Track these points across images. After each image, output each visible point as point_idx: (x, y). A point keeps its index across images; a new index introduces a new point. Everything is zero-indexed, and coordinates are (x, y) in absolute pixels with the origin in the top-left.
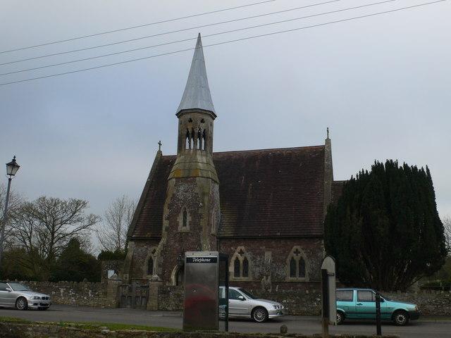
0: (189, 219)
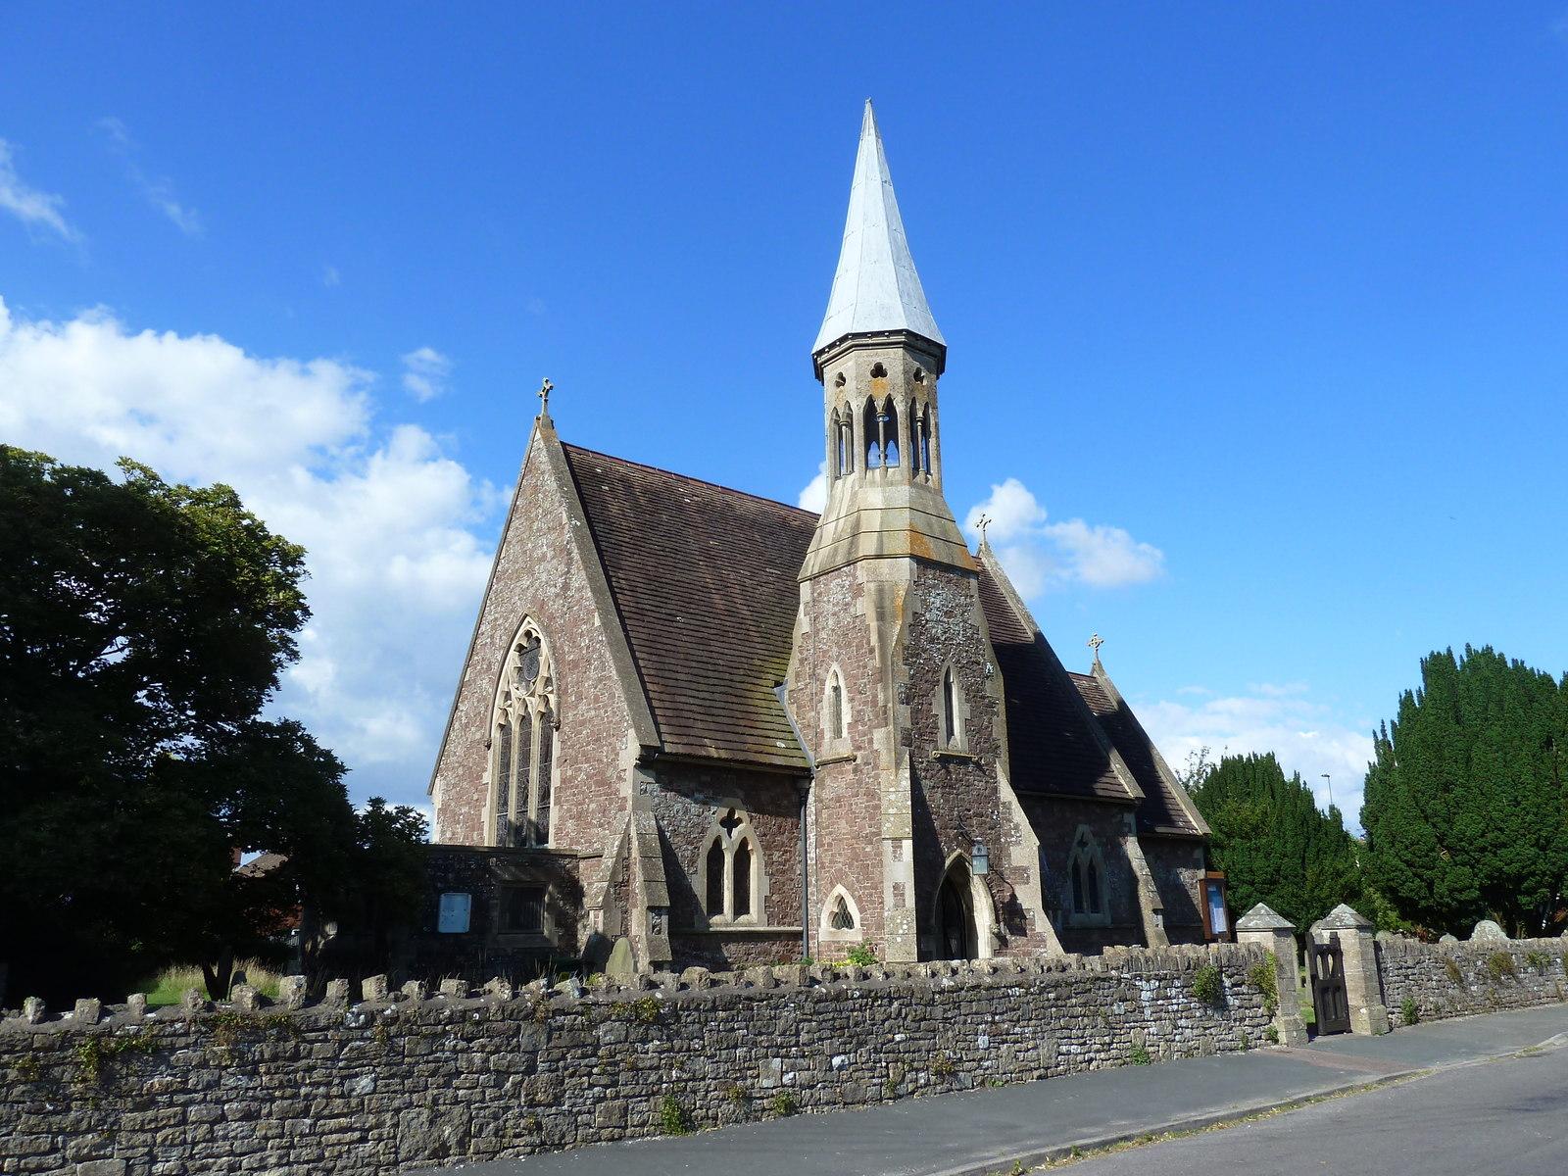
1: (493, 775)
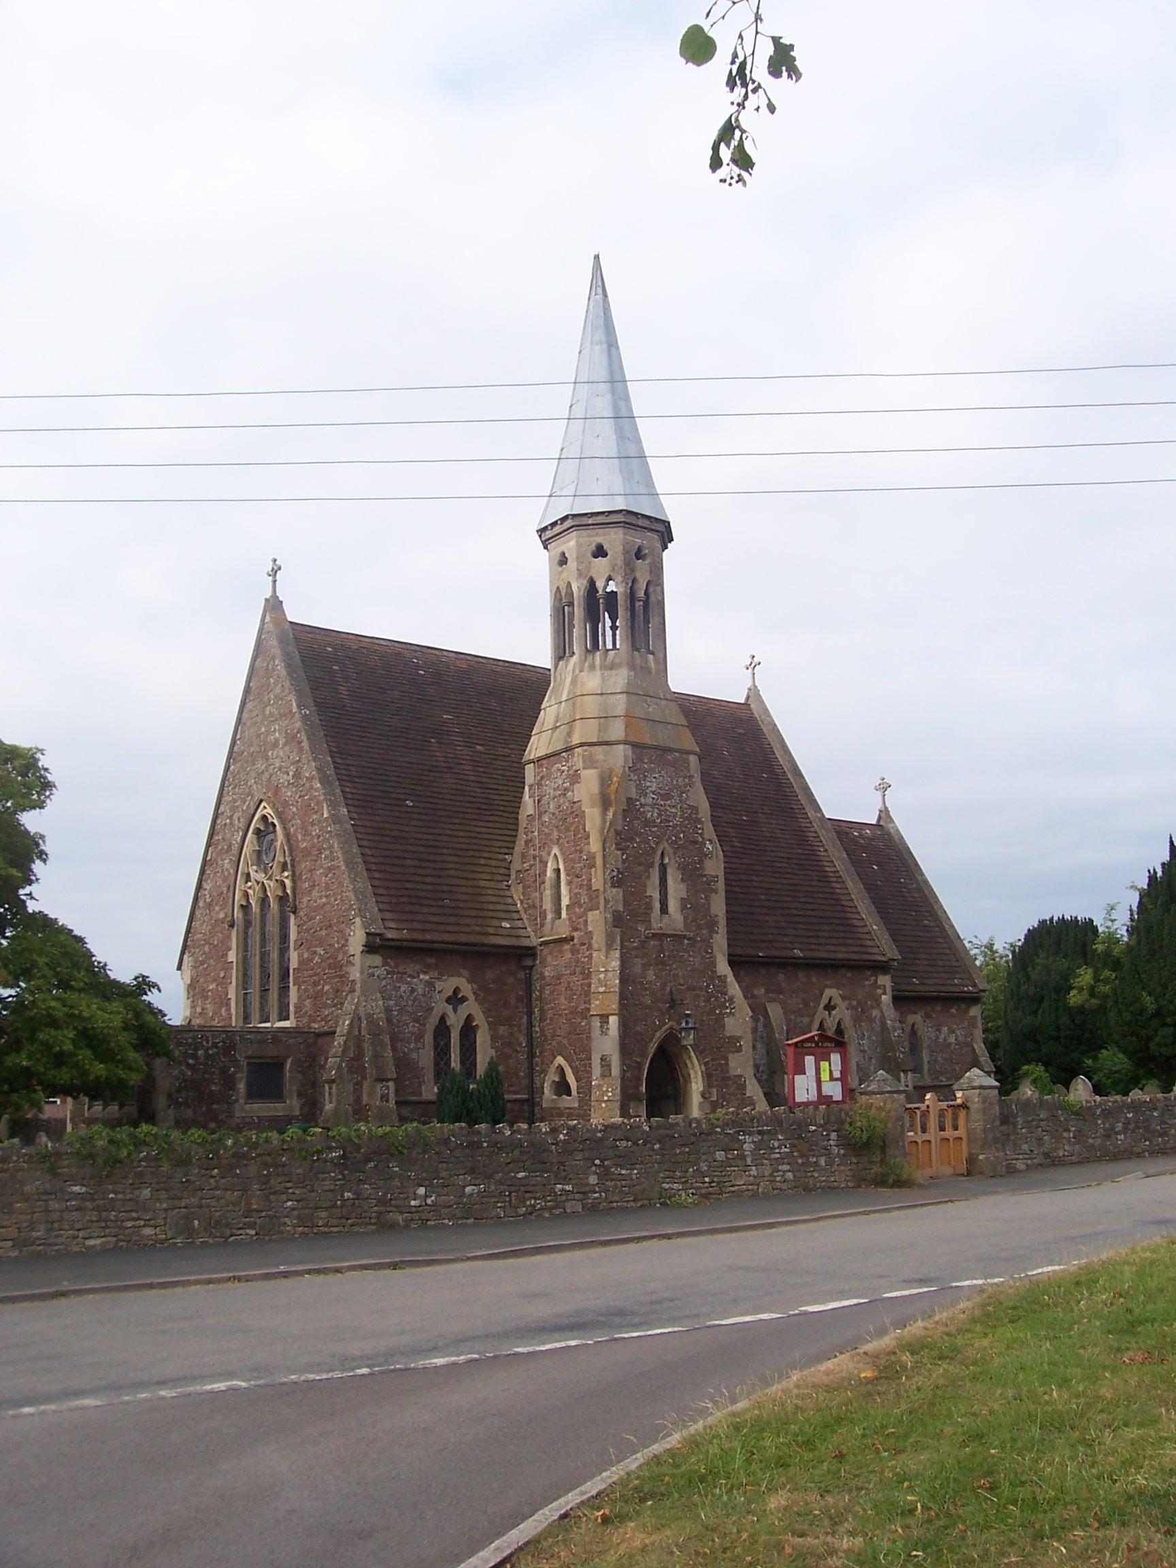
0: (677, 890)
1: (237, 954)
